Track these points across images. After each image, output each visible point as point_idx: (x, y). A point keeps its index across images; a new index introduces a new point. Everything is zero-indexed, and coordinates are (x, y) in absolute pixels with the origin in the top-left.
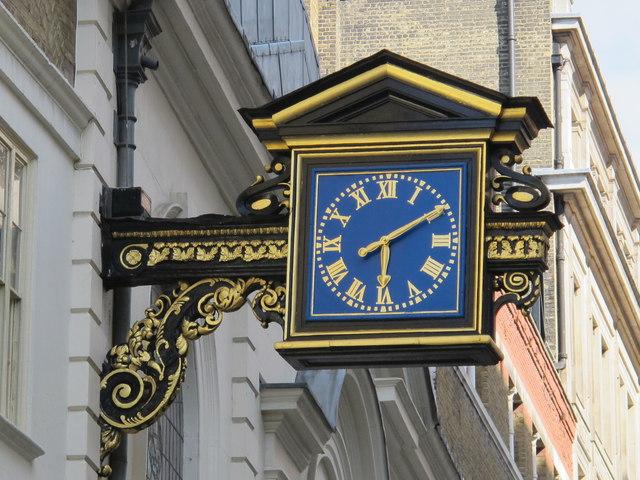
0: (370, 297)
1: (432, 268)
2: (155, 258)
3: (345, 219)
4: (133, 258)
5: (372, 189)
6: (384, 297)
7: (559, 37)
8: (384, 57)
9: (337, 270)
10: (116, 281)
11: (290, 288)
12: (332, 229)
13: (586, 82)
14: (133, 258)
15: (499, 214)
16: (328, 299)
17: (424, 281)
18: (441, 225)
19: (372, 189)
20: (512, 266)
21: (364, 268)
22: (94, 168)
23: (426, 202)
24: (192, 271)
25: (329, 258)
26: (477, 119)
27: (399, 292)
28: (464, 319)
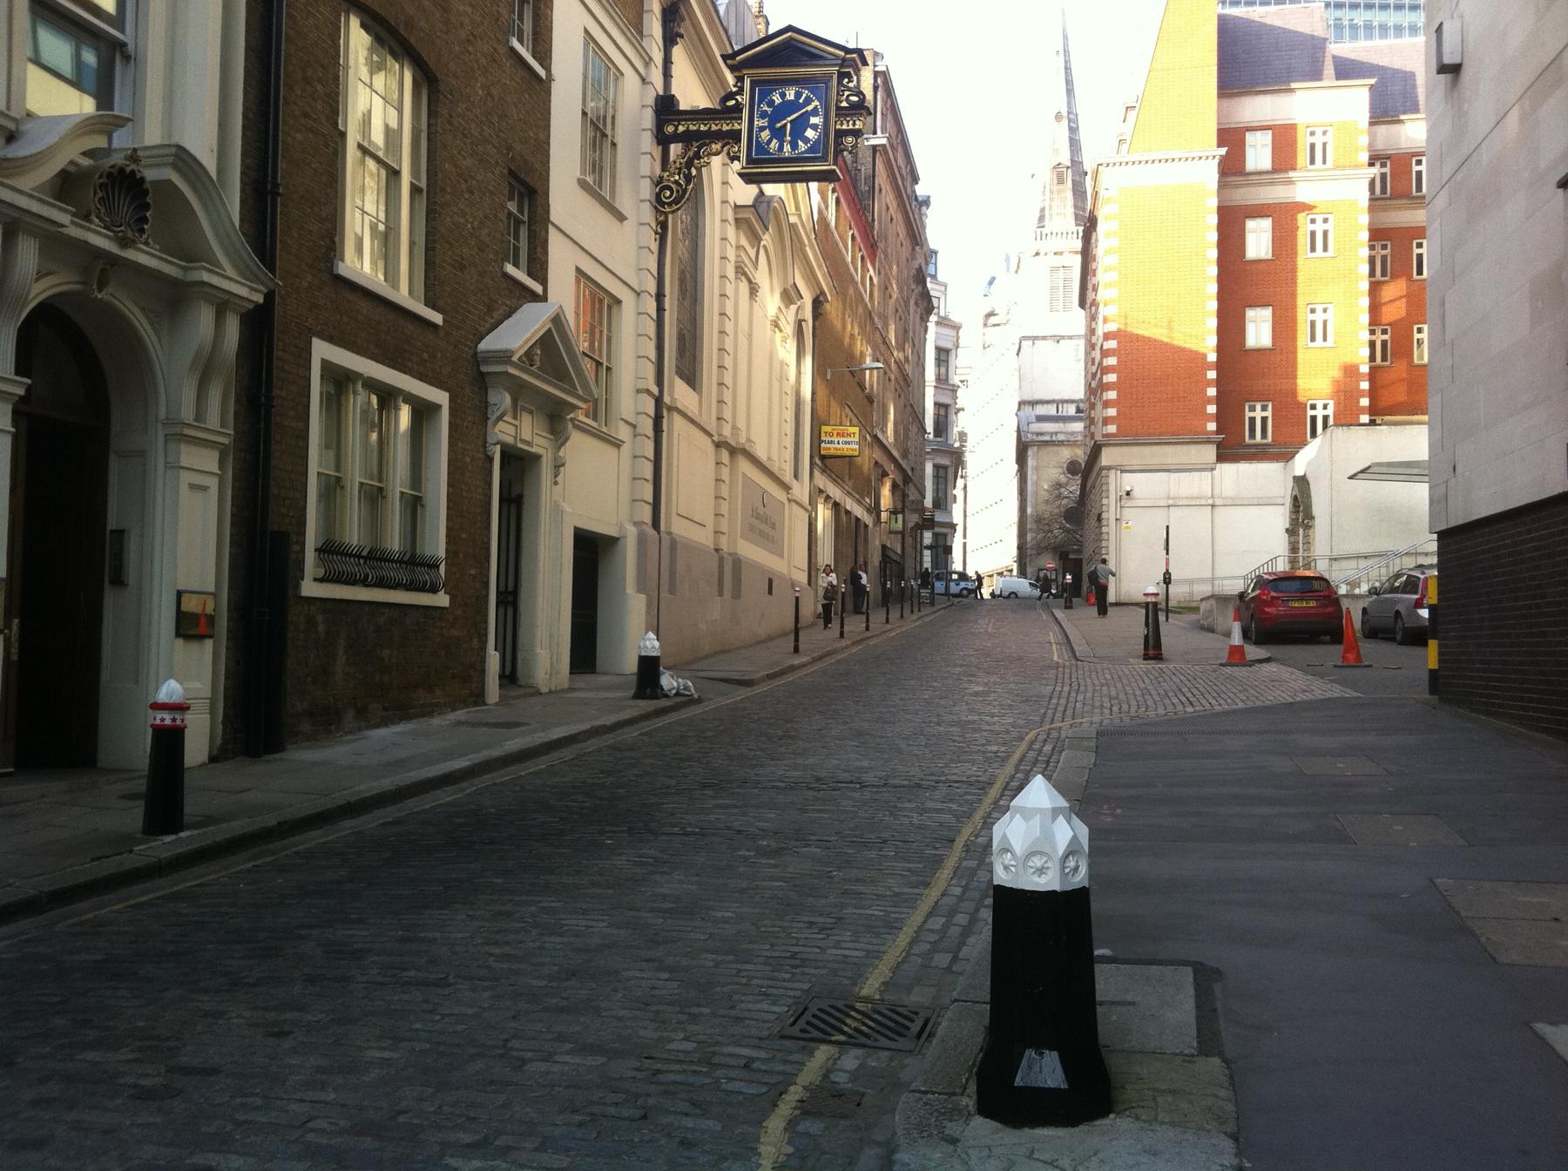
0: (781, 148)
1: (810, 133)
2: (681, 129)
3: (769, 110)
4: (670, 129)
5: (783, 95)
6: (787, 148)
8: (790, 28)
9: (765, 135)
14: (670, 129)
16: (762, 148)
17: (806, 140)
18: (815, 112)
19: (783, 95)
21: (778, 134)
23: (808, 101)
25: (762, 129)
27: (794, 146)
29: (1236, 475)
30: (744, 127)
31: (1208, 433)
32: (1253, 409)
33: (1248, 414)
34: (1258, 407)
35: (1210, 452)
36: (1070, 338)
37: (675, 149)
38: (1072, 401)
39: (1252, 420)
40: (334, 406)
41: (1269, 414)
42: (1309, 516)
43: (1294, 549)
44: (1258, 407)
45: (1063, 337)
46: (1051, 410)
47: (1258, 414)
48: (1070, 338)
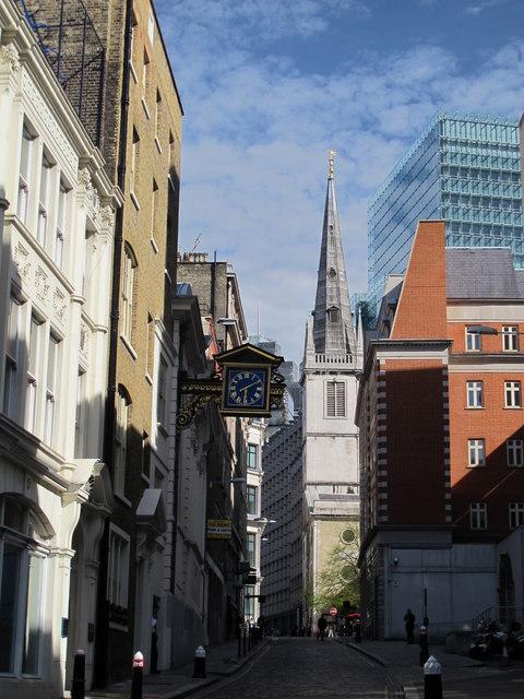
0: (242, 401)
1: (257, 395)
4: (185, 388)
5: (243, 375)
6: (245, 401)
7: (229, 279)
9: (234, 394)
10: (180, 392)
11: (223, 397)
12: (233, 384)
13: (234, 292)
14: (185, 388)
15: (362, 506)
16: (232, 401)
18: (259, 385)
19: (243, 375)
20: (275, 396)
21: (241, 394)
22: (119, 213)
23: (256, 379)
24: (199, 392)
26: (269, 361)
27: (249, 401)
28: (264, 408)
29: (463, 553)
30: (223, 389)
31: (447, 523)
32: (513, 507)
33: (511, 510)
34: (517, 505)
35: (448, 538)
36: (343, 435)
37: (187, 398)
38: (345, 484)
39: (513, 514)
40: (108, 476)
41: (485, 510)
42: (511, 581)
43: (502, 602)
44: (517, 505)
45: (338, 435)
46: (329, 490)
47: (517, 510)
48: (343, 435)
